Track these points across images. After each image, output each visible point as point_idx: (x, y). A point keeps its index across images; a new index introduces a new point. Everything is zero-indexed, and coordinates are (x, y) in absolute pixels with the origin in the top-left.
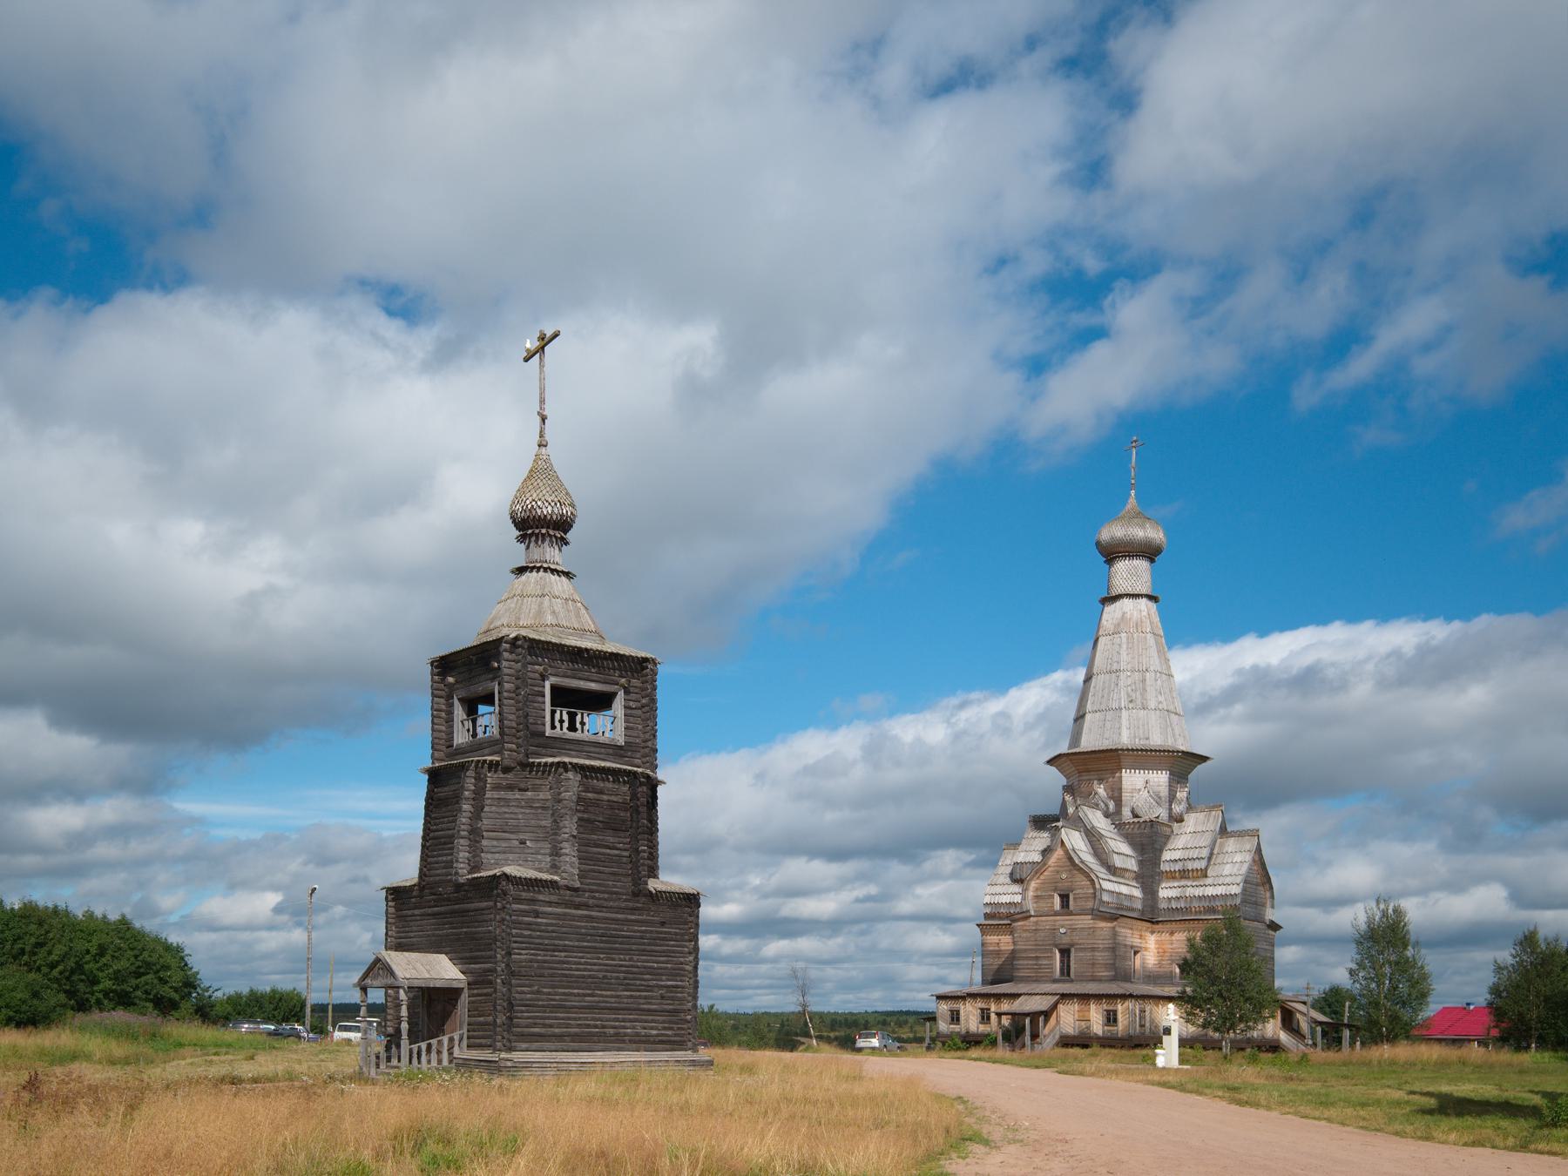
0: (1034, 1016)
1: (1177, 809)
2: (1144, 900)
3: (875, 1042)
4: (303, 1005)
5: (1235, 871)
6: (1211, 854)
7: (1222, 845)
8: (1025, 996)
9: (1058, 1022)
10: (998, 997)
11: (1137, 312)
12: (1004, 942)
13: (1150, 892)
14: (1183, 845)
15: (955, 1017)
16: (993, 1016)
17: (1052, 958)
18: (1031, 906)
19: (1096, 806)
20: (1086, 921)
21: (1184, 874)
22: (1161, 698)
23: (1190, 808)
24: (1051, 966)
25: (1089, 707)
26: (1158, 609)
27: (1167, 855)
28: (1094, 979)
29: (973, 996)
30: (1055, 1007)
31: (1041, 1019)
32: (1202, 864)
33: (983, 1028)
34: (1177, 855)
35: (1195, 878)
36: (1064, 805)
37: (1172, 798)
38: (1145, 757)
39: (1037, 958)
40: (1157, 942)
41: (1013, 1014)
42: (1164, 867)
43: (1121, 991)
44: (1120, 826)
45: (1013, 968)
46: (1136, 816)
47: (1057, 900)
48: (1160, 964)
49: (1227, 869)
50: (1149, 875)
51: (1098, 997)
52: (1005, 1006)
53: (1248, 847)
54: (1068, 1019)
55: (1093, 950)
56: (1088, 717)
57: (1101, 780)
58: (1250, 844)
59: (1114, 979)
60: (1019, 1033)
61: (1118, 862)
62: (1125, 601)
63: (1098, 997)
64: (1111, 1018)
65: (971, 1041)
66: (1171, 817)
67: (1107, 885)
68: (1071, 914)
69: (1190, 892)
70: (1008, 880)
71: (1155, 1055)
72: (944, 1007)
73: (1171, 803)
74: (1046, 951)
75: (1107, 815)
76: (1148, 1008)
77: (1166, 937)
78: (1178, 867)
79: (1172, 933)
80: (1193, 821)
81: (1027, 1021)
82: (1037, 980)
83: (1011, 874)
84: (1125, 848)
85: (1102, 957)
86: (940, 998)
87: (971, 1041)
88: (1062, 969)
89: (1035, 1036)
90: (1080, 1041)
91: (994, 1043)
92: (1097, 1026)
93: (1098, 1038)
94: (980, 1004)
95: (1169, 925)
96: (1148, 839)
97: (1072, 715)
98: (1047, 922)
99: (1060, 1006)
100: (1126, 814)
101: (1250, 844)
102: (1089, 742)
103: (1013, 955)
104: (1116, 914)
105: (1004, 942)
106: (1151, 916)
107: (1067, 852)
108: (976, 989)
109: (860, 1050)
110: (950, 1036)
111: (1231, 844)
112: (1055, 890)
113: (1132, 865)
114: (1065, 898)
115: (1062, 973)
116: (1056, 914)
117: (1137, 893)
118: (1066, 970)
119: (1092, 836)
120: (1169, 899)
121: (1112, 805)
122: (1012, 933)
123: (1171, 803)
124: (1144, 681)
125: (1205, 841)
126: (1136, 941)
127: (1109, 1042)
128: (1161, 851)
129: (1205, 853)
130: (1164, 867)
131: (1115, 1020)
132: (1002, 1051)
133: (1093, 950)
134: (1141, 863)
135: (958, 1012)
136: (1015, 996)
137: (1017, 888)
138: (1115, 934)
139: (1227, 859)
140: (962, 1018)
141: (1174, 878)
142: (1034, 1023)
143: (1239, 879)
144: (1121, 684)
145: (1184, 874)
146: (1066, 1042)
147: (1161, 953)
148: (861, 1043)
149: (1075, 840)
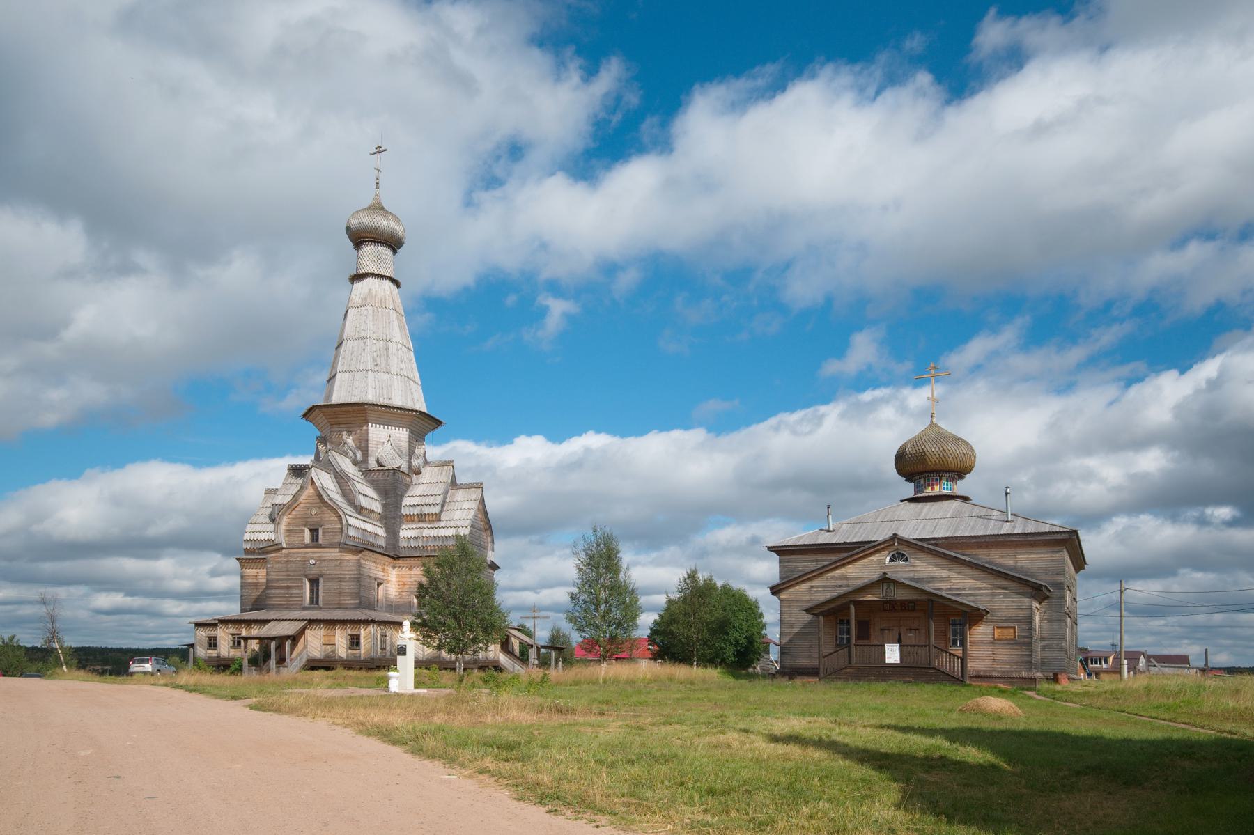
0: (281, 640)
1: (416, 462)
3: (148, 667)
7: (453, 495)
9: (305, 647)
12: (259, 574)
13: (393, 532)
15: (213, 643)
17: (301, 587)
18: (283, 540)
19: (345, 454)
20: (334, 553)
21: (421, 518)
22: (403, 366)
24: (301, 596)
25: (339, 367)
28: (340, 607)
30: (302, 632)
31: (288, 643)
32: (437, 509)
33: (233, 653)
37: (411, 453)
38: (390, 414)
42: (405, 511)
43: (364, 617)
44: (366, 473)
47: (307, 534)
49: (457, 515)
50: (392, 517)
51: (343, 622)
52: (256, 631)
53: (474, 497)
54: (314, 643)
55: (340, 580)
56: (338, 376)
57: (350, 433)
58: (475, 494)
59: (359, 606)
61: (364, 502)
63: (343, 622)
64: (355, 642)
65: (222, 666)
66: (410, 468)
67: (352, 521)
68: (320, 547)
69: (426, 533)
70: (267, 520)
72: (203, 633)
74: (296, 581)
75: (355, 463)
77: (405, 571)
78: (416, 511)
79: (411, 568)
82: (288, 608)
84: (370, 492)
85: (348, 586)
86: (198, 625)
87: (222, 666)
88: (311, 598)
90: (325, 665)
94: (231, 629)
95: (408, 561)
96: (391, 485)
98: (298, 554)
99: (308, 631)
100: (372, 464)
101: (475, 494)
103: (269, 584)
104: (362, 548)
105: (259, 574)
106: (394, 554)
107: (317, 490)
109: (132, 674)
111: (460, 495)
113: (377, 507)
114: (314, 532)
115: (311, 601)
116: (307, 547)
118: (314, 599)
121: (359, 456)
124: (387, 349)
125: (439, 489)
126: (380, 574)
127: (349, 664)
128: (402, 497)
129: (439, 500)
130: (405, 511)
131: (358, 644)
132: (250, 676)
133: (340, 580)
134: (384, 506)
138: (360, 566)
139: (457, 506)
141: (413, 521)
142: (280, 648)
143: (467, 523)
144: (368, 349)
145: (421, 518)
146: (313, 665)
147: (402, 586)
148: (134, 668)
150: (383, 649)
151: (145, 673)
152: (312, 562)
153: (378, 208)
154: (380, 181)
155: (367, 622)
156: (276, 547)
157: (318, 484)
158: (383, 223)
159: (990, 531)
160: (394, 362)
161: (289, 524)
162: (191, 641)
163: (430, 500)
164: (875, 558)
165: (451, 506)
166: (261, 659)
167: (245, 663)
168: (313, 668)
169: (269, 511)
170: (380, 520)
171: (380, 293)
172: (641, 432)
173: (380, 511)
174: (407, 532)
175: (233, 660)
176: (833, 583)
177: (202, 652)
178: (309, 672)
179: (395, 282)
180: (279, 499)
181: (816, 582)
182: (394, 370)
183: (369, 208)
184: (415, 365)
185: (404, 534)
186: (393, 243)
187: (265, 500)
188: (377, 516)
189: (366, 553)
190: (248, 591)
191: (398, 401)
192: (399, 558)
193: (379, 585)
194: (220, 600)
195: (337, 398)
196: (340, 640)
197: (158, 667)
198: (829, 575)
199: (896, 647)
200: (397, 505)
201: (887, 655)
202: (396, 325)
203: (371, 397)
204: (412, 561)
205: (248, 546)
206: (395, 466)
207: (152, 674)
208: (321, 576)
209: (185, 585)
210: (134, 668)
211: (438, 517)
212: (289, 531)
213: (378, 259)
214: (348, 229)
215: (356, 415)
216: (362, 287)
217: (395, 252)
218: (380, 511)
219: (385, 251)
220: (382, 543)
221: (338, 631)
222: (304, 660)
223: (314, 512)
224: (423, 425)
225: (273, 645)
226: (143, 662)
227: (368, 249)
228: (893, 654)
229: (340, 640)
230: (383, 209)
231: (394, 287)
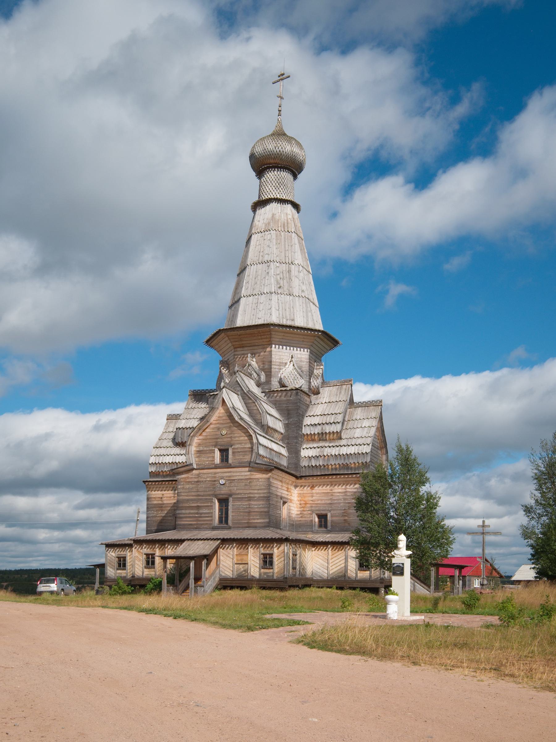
0: (198, 559)
1: (315, 383)
2: (289, 458)
3: (54, 587)
5: (364, 434)
6: (344, 420)
7: (351, 414)
8: (177, 552)
9: (218, 565)
10: (163, 543)
12: (167, 497)
13: (294, 451)
14: (321, 411)
15: (122, 563)
16: (158, 560)
17: (211, 507)
18: (194, 461)
19: (250, 376)
20: (244, 473)
21: (322, 437)
22: (304, 288)
23: (324, 383)
24: (211, 515)
25: (244, 292)
26: (298, 216)
27: (307, 421)
28: (249, 526)
29: (139, 542)
30: (215, 551)
31: (204, 562)
32: (338, 428)
33: (148, 573)
34: (316, 420)
35: (331, 440)
36: (221, 378)
37: (311, 374)
38: (291, 334)
39: (198, 507)
40: (300, 495)
41: (177, 558)
42: (306, 431)
43: (277, 536)
44: (269, 393)
45: (175, 517)
46: (283, 385)
47: (217, 454)
49: (358, 433)
50: (293, 438)
51: (256, 541)
52: (169, 551)
53: (374, 414)
54: (227, 563)
55: (250, 499)
56: (243, 301)
57: (253, 354)
58: (374, 412)
59: (268, 525)
60: (183, 575)
61: (271, 422)
62: (274, 205)
63: (256, 541)
64: (267, 561)
65: (138, 586)
66: (310, 389)
67: (262, 441)
68: (230, 467)
69: (328, 451)
70: (171, 444)
71: (386, 603)
72: (113, 554)
73: (310, 377)
74: (206, 501)
75: (259, 385)
76: (298, 552)
77: (307, 490)
78: (317, 430)
79: (313, 487)
80: (326, 394)
81: (192, 564)
82: (198, 528)
83: (174, 439)
84: (273, 412)
85: (257, 505)
86: (109, 546)
87: (138, 586)
88: (220, 518)
89: (198, 579)
90: (240, 583)
91: (158, 588)
92: (254, 568)
93: (253, 580)
94: (146, 550)
95: (311, 480)
96: (293, 404)
97: (229, 302)
99: (220, 551)
100: (275, 385)
101: (374, 412)
102: (243, 319)
103: (176, 506)
104: (271, 467)
105: (167, 497)
106: (297, 473)
107: (227, 410)
108: (142, 534)
109: (41, 593)
110: (115, 581)
111: (359, 413)
113: (279, 426)
114: (224, 452)
115: (220, 521)
116: (216, 467)
117: (284, 451)
118: (224, 518)
119: (247, 398)
121: (263, 378)
122: (174, 489)
123: (310, 377)
124: (289, 271)
125: (340, 408)
126: (284, 493)
127: (266, 584)
128: (303, 416)
129: (340, 418)
130: (306, 431)
131: (271, 563)
132: (168, 598)
133: (250, 499)
134: (287, 426)
135: (124, 558)
136: (179, 542)
137: (177, 450)
138: (269, 485)
139: (356, 424)
140: (128, 564)
141: (313, 440)
142: (198, 569)
143: (369, 440)
144: (272, 272)
145: (322, 437)
146: (226, 585)
147: (303, 505)
148: (41, 588)
149: (234, 400)
150: (294, 568)
151: (52, 592)
153: (279, 134)
154: (282, 109)
156: (187, 468)
157: (229, 404)
158: (287, 148)
160: (296, 283)
161: (199, 445)
162: (102, 561)
163: (331, 419)
165: (351, 424)
166: (177, 577)
167: (165, 581)
168: (225, 588)
169: (172, 436)
170: (282, 440)
171: (283, 217)
172: (438, 376)
173: (282, 431)
174: (307, 452)
175: (149, 580)
177: (111, 572)
178: (223, 592)
179: (296, 206)
180: (182, 424)
182: (296, 292)
183: (273, 134)
184: (313, 288)
185: (304, 453)
186: (294, 167)
187: (167, 426)
188: (280, 436)
189: (276, 472)
190: (153, 513)
191: (300, 322)
192: (301, 477)
193: (284, 503)
194: (85, 529)
195: (240, 322)
196: (253, 560)
197: (62, 587)
200: (299, 425)
202: (297, 247)
203: (275, 319)
204: (315, 480)
205: (153, 469)
206: (297, 386)
207: (57, 593)
208: (230, 495)
209: (54, 517)
210: (41, 588)
211: (338, 436)
212: (199, 452)
213: (280, 184)
214: (252, 157)
215: (262, 336)
216: (265, 213)
217: (295, 177)
218: (282, 431)
219: (286, 175)
220: (284, 463)
221: (251, 550)
222: (217, 579)
223: (224, 432)
224: (321, 343)
225: (192, 564)
226: (48, 581)
227: (271, 175)
229: (253, 560)
230: (285, 134)
231: (294, 211)
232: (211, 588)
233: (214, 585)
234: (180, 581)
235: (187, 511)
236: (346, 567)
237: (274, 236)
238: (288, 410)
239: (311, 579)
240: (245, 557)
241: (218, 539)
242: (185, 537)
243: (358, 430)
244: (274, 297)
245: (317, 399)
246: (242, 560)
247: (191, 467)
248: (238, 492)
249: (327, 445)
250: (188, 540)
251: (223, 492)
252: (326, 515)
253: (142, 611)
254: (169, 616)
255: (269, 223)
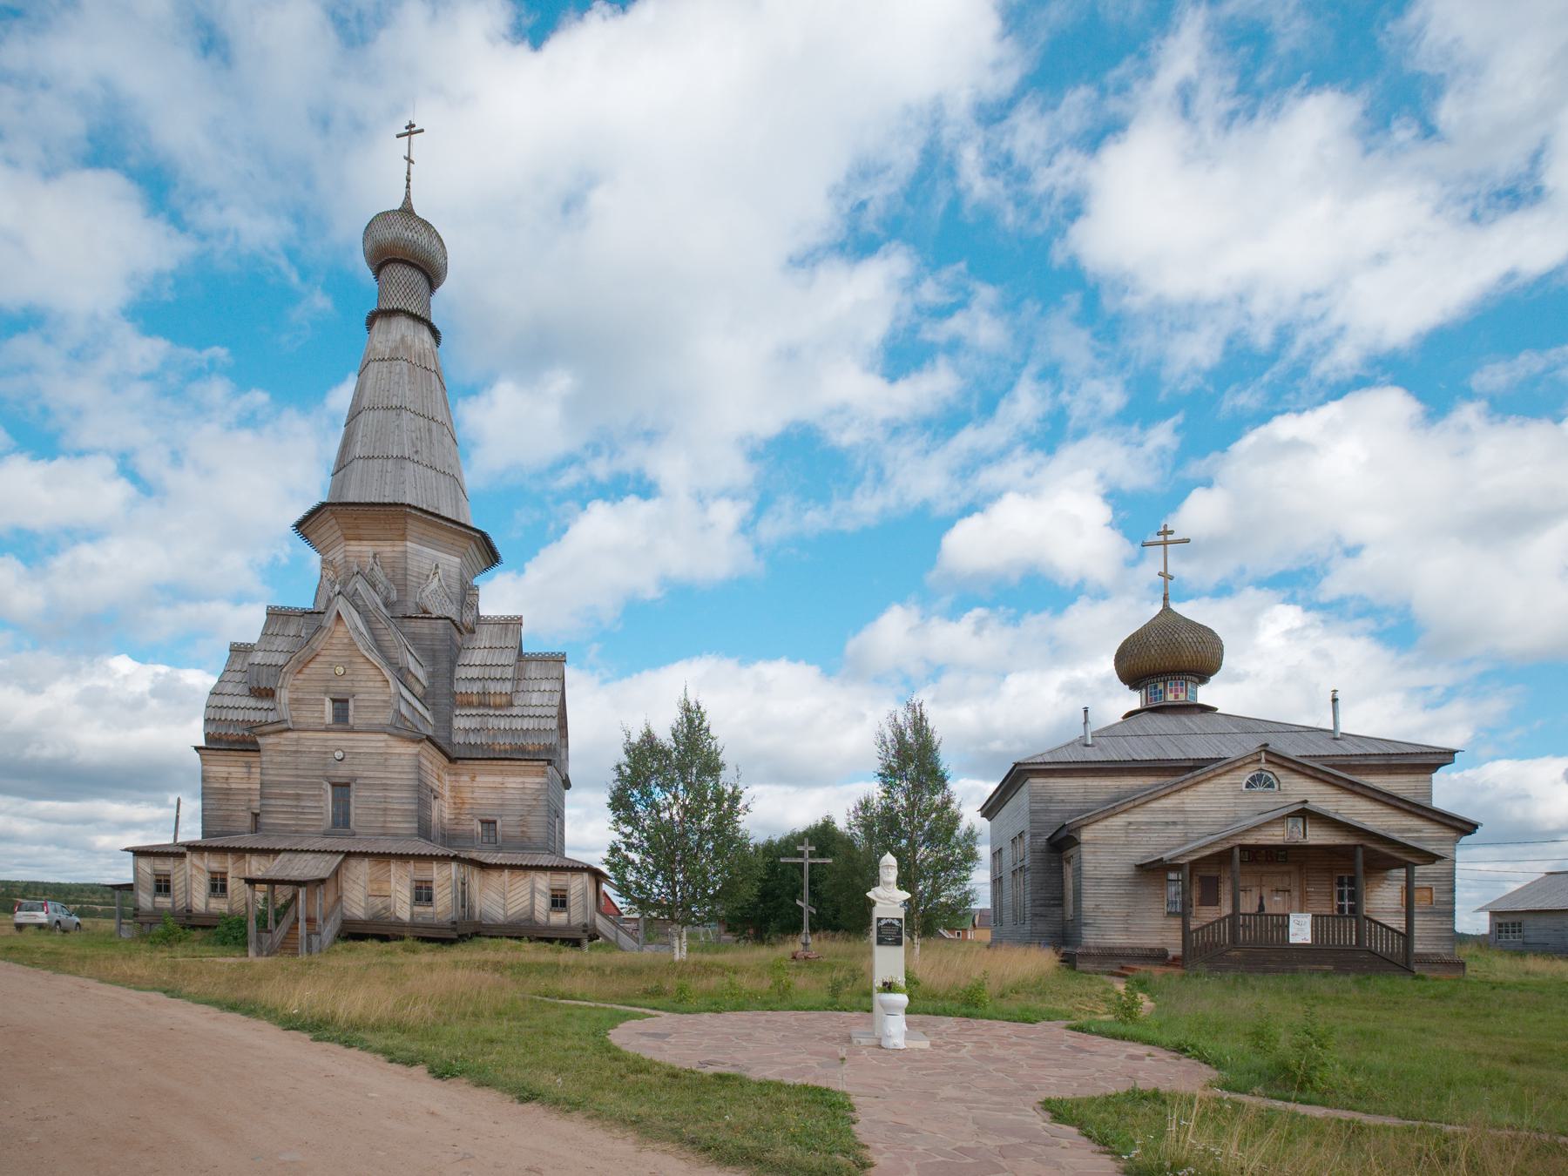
4: (813, 930)
11: (19, 920)
15: (163, 886)
20: (378, 742)
21: (483, 702)
25: (358, 450)
27: (461, 673)
32: (507, 687)
34: (474, 673)
39: (298, 797)
42: (461, 687)
48: (457, 819)
49: (535, 699)
52: (257, 867)
63: (403, 857)
64: (423, 894)
68: (352, 730)
69: (492, 723)
78: (476, 688)
92: (403, 907)
94: (213, 863)
98: (313, 741)
110: (157, 915)
112: (326, 693)
114: (341, 704)
116: (327, 730)
118: (342, 820)
120: (467, 731)
127: (547, 936)
129: (509, 673)
134: (432, 676)
139: (531, 685)
145: (483, 702)
152: (339, 755)
155: (445, 859)
159: (1052, 780)
163: (498, 673)
164: (1225, 780)
173: (425, 683)
175: (220, 917)
176: (1162, 818)
181: (1138, 816)
185: (459, 723)
198: (1154, 805)
199: (1307, 919)
201: (1292, 930)
222: (338, 922)
227: (398, 273)
228: (1301, 930)
232: (331, 937)
233: (334, 931)
234: (277, 923)
235: (279, 802)
236: (532, 905)
237: (405, 370)
238: (434, 651)
239: (479, 924)
240: (385, 886)
241: (337, 852)
242: (282, 846)
243: (535, 695)
244: (409, 465)
245: (471, 640)
246: (379, 889)
247: (285, 726)
248: (366, 774)
249: (491, 712)
250: (285, 850)
251: (340, 773)
252: (495, 822)
253: (291, 1024)
254: (411, 1063)
255: (397, 348)
